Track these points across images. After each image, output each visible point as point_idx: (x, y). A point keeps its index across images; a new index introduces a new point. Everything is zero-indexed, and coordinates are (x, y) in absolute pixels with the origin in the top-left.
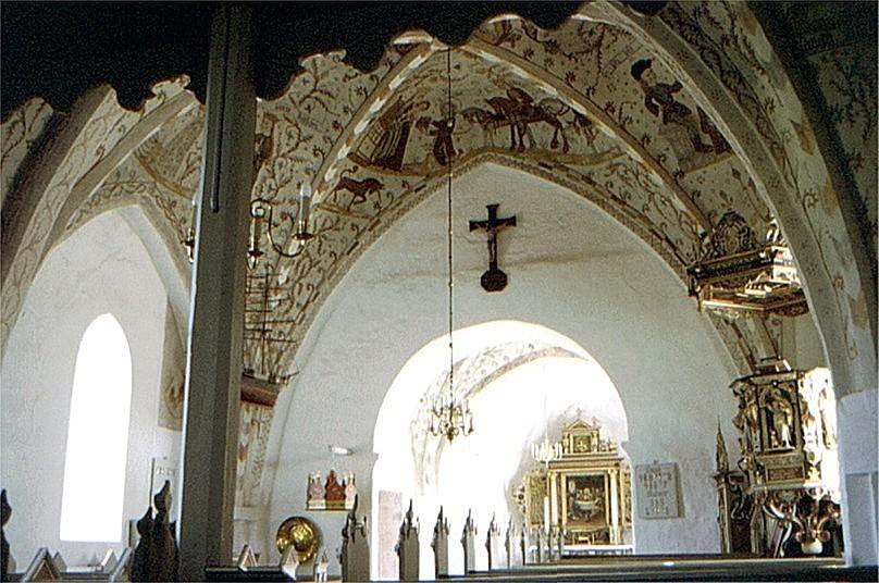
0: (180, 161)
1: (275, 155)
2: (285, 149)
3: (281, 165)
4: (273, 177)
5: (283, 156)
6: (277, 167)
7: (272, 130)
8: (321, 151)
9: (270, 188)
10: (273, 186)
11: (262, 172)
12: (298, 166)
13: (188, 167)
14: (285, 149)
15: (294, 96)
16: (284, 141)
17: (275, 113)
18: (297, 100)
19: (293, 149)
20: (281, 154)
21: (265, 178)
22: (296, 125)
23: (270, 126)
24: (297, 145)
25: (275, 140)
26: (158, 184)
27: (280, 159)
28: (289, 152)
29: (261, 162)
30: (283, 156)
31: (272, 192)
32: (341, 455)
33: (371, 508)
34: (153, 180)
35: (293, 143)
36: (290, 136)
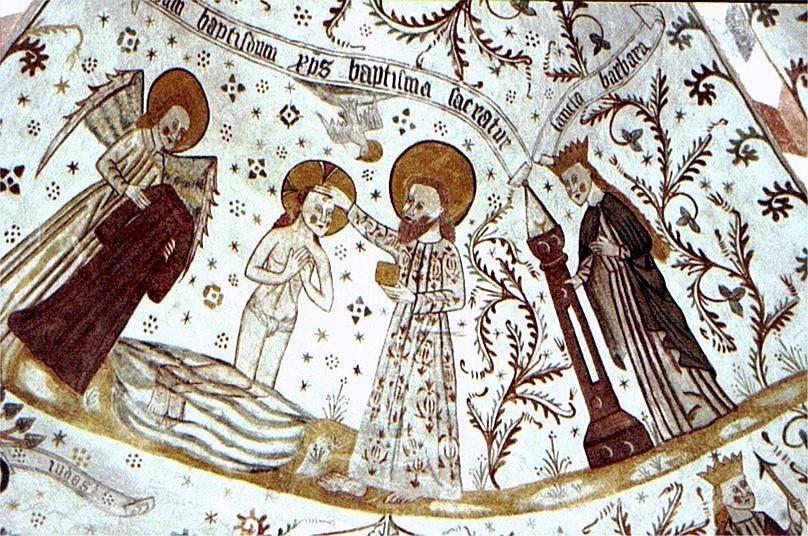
0: (452, 433)
1: (650, 213)
2: (653, 177)
3: (687, 219)
4: (708, 264)
5: (668, 191)
6: (687, 234)
7: (595, 176)
8: (707, 72)
9: (732, 297)
10: (734, 284)
11: (677, 282)
12: (718, 168)
13: (490, 437)
14: (653, 177)
15: (555, 64)
16: (630, 161)
17: (565, 141)
18: (566, 62)
19: (665, 153)
20: (657, 192)
21: (695, 290)
22: (620, 104)
23: (584, 175)
24: (661, 136)
25: (624, 187)
26: (399, 520)
27: (672, 214)
28: (664, 169)
29: (651, 267)
30: (668, 191)
31: (746, 301)
32: (162, 247)
33: (63, 286)
34: (375, 517)
35: (650, 143)
36: (632, 139)
